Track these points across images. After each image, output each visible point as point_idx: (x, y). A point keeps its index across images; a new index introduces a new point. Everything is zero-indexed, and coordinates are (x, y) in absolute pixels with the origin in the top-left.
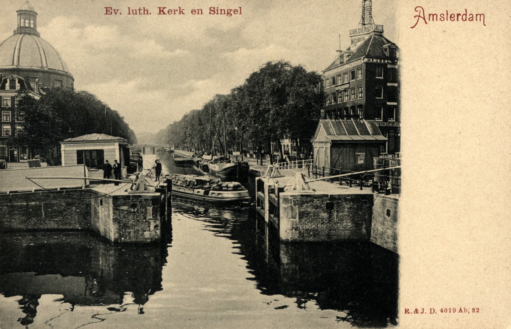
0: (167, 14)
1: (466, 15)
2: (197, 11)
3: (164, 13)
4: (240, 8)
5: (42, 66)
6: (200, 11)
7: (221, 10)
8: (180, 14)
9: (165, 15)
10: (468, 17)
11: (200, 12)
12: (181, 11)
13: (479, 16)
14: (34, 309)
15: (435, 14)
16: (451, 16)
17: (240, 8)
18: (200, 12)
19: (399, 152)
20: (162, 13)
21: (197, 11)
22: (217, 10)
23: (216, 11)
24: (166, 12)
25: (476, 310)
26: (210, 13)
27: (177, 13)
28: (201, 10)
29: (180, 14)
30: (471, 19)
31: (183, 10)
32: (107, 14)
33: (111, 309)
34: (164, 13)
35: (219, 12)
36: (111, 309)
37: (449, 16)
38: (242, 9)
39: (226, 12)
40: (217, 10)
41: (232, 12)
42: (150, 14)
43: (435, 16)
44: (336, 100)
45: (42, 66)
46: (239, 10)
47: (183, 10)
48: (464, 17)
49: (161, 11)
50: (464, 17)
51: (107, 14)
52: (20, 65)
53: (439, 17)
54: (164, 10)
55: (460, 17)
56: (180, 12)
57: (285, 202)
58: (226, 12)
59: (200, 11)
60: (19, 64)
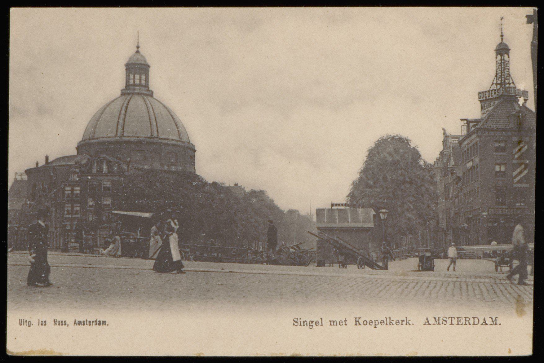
0: (395, 324)
3: (360, 324)
4: (321, 319)
5: (152, 135)
7: (304, 322)
8: (407, 324)
9: (394, 326)
12: (408, 321)
16: (340, 323)
17: (321, 319)
20: (408, 324)
22: (300, 322)
23: (299, 323)
24: (361, 323)
26: (294, 324)
27: (404, 323)
29: (407, 324)
30: (100, 324)
31: (409, 321)
32: (458, 324)
35: (302, 324)
38: (323, 320)
39: (308, 324)
40: (300, 322)
41: (314, 324)
42: (500, 324)
45: (152, 135)
46: (320, 321)
47: (409, 321)
48: (377, 323)
49: (357, 323)
50: (377, 323)
51: (458, 324)
52: (125, 134)
54: (359, 321)
55: (94, 323)
56: (407, 323)
57: (341, 267)
58: (308, 324)
60: (123, 135)
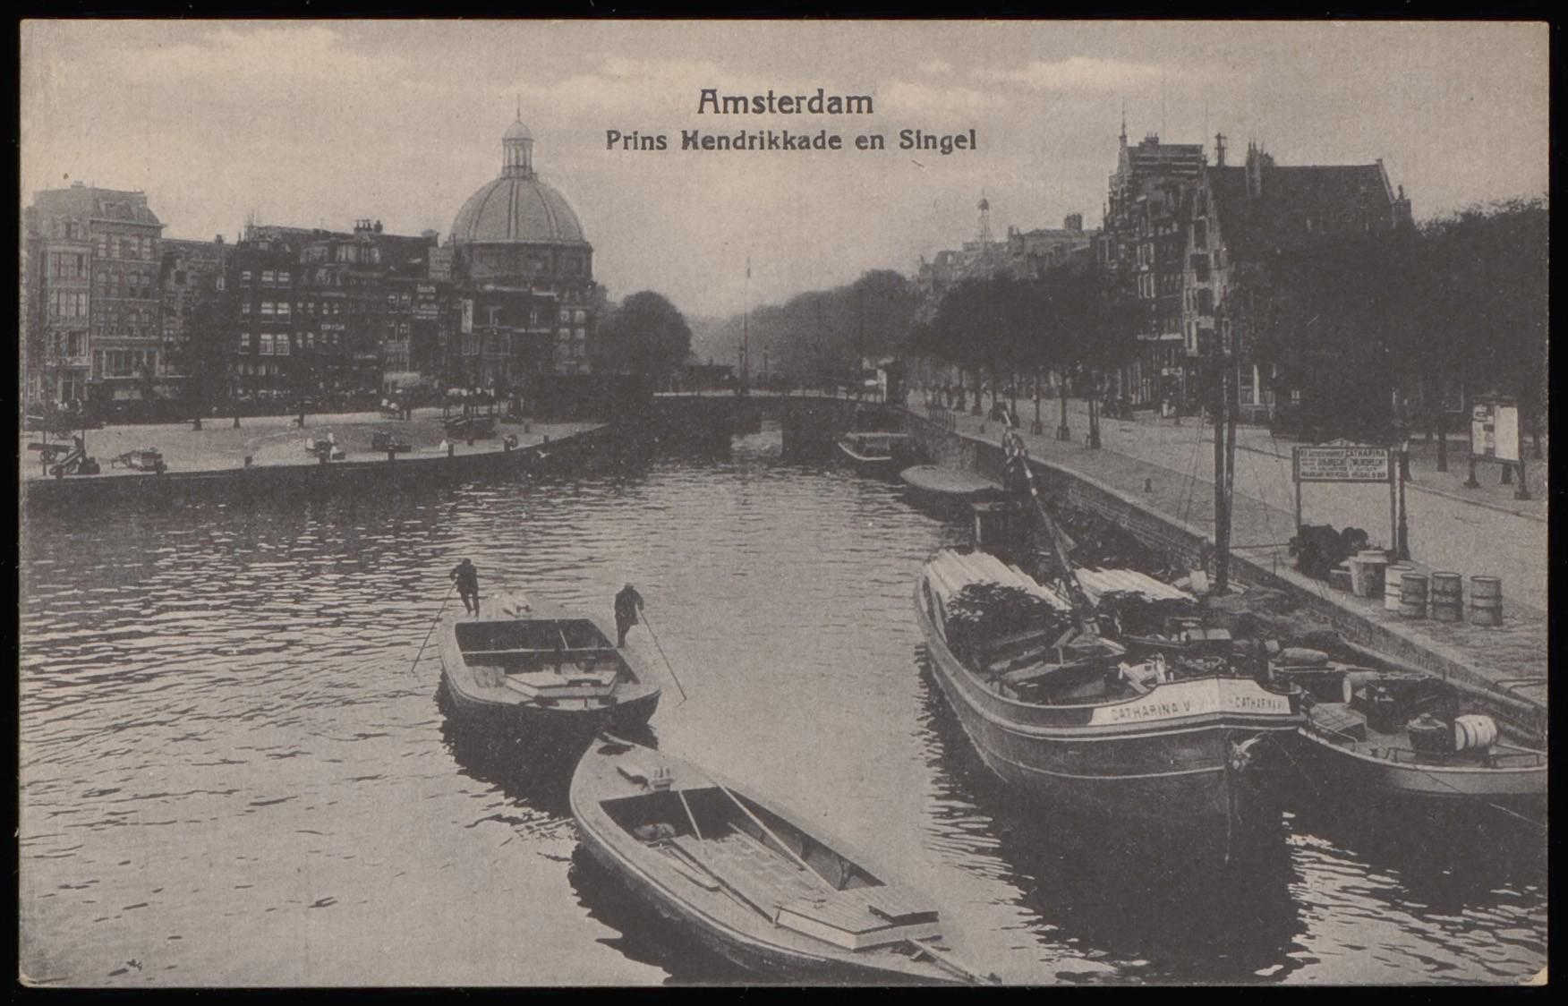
1: (820, 98)
2: (844, 102)
3: (793, 147)
6: (877, 141)
10: (826, 103)
11: (877, 144)
13: (731, 104)
14: (636, 830)
15: (864, 98)
18: (877, 144)
19: (703, 837)
20: (789, 146)
21: (844, 102)
25: (539, 854)
28: (869, 100)
33: (1488, 951)
34: (793, 147)
36: (1488, 951)
37: (775, 103)
43: (741, 103)
44: (33, 668)
46: (968, 137)
53: (751, 106)
59: (877, 141)
